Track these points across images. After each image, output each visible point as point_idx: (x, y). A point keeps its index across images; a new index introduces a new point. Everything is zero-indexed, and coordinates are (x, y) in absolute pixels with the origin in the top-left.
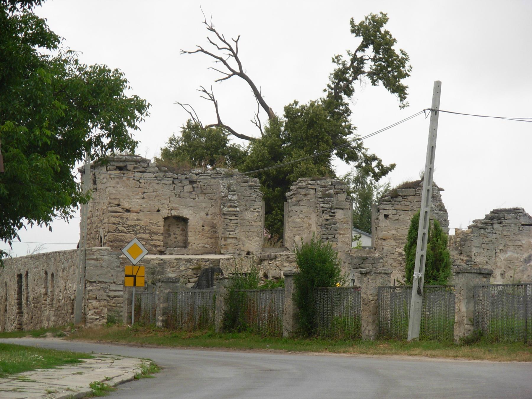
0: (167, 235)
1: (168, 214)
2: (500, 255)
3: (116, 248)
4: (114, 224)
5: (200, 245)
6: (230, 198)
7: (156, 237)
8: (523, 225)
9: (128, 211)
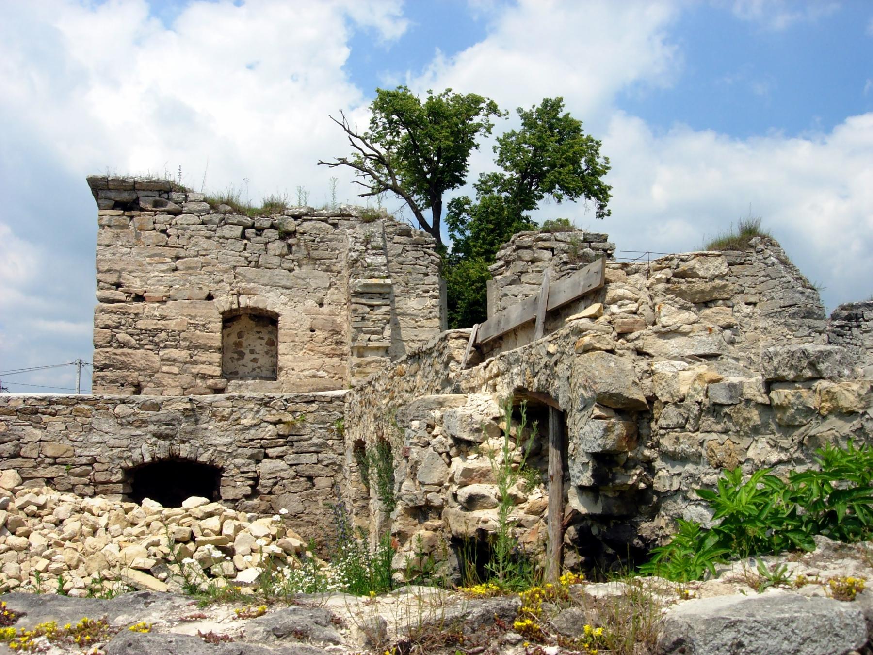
0: (236, 356)
1: (232, 303)
3: (112, 382)
4: (107, 327)
5: (307, 373)
6: (369, 261)
7: (204, 356)
9: (139, 298)
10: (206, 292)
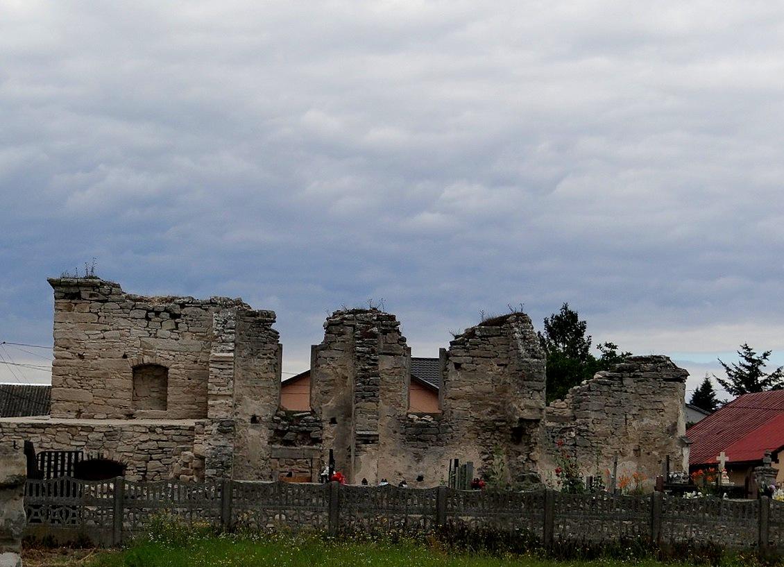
2: (634, 424)
6: (223, 338)
8: (665, 380)
10: (122, 353)
